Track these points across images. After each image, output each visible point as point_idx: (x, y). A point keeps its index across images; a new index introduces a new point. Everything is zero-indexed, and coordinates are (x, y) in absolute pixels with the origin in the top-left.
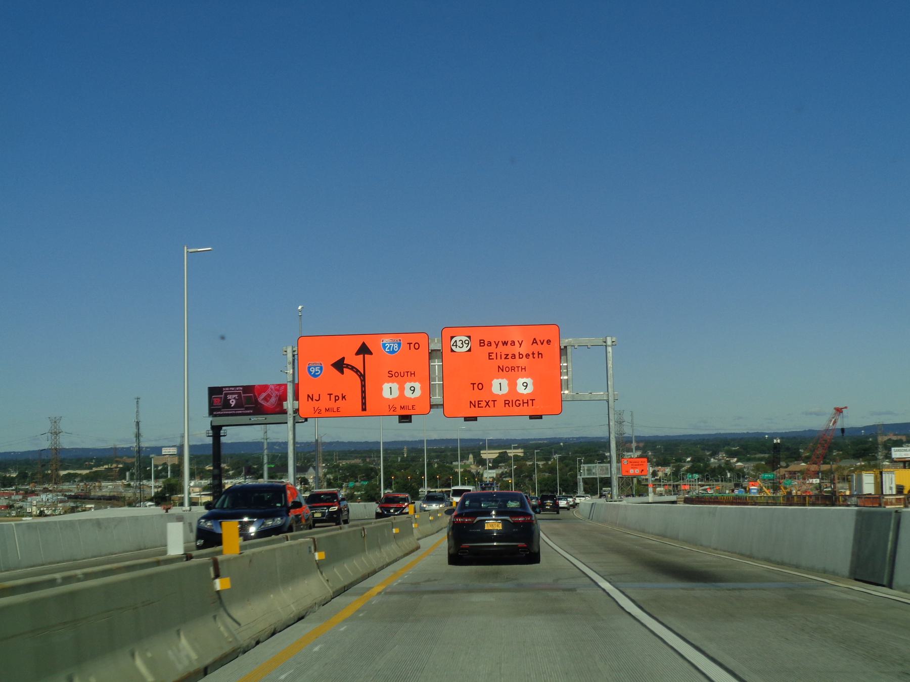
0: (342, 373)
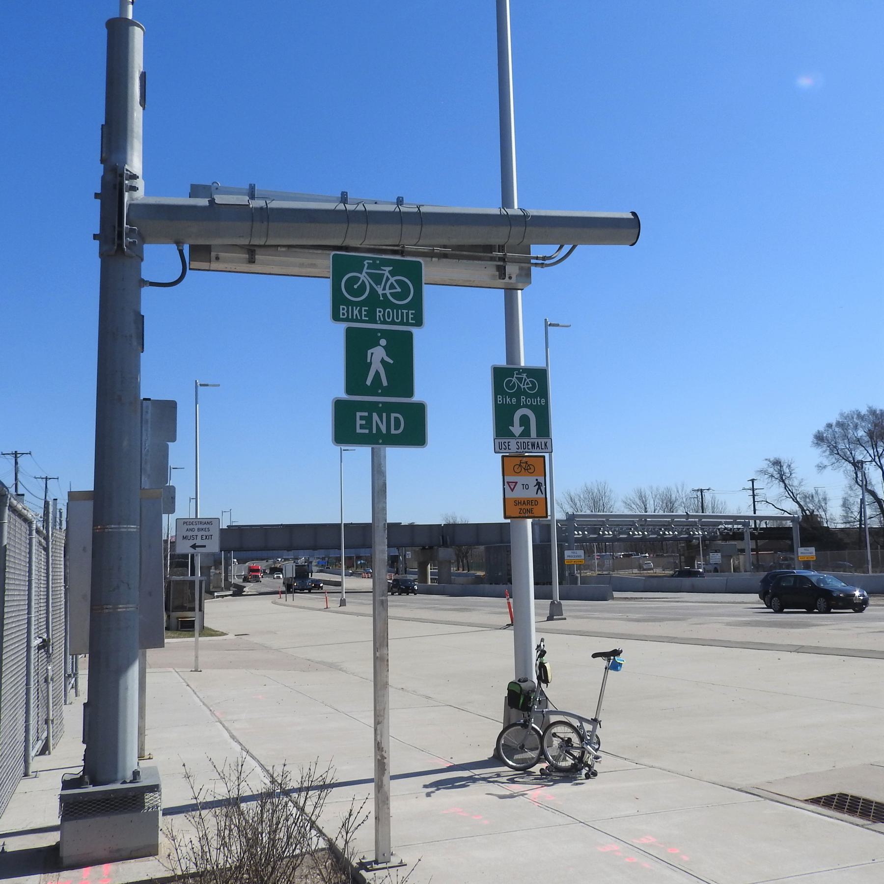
0: (195, 549)
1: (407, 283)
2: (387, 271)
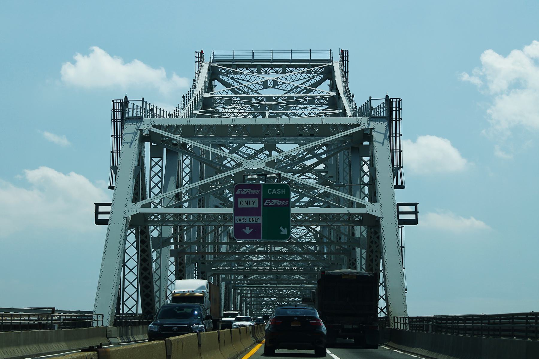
1: (236, 238)
2: (274, 192)
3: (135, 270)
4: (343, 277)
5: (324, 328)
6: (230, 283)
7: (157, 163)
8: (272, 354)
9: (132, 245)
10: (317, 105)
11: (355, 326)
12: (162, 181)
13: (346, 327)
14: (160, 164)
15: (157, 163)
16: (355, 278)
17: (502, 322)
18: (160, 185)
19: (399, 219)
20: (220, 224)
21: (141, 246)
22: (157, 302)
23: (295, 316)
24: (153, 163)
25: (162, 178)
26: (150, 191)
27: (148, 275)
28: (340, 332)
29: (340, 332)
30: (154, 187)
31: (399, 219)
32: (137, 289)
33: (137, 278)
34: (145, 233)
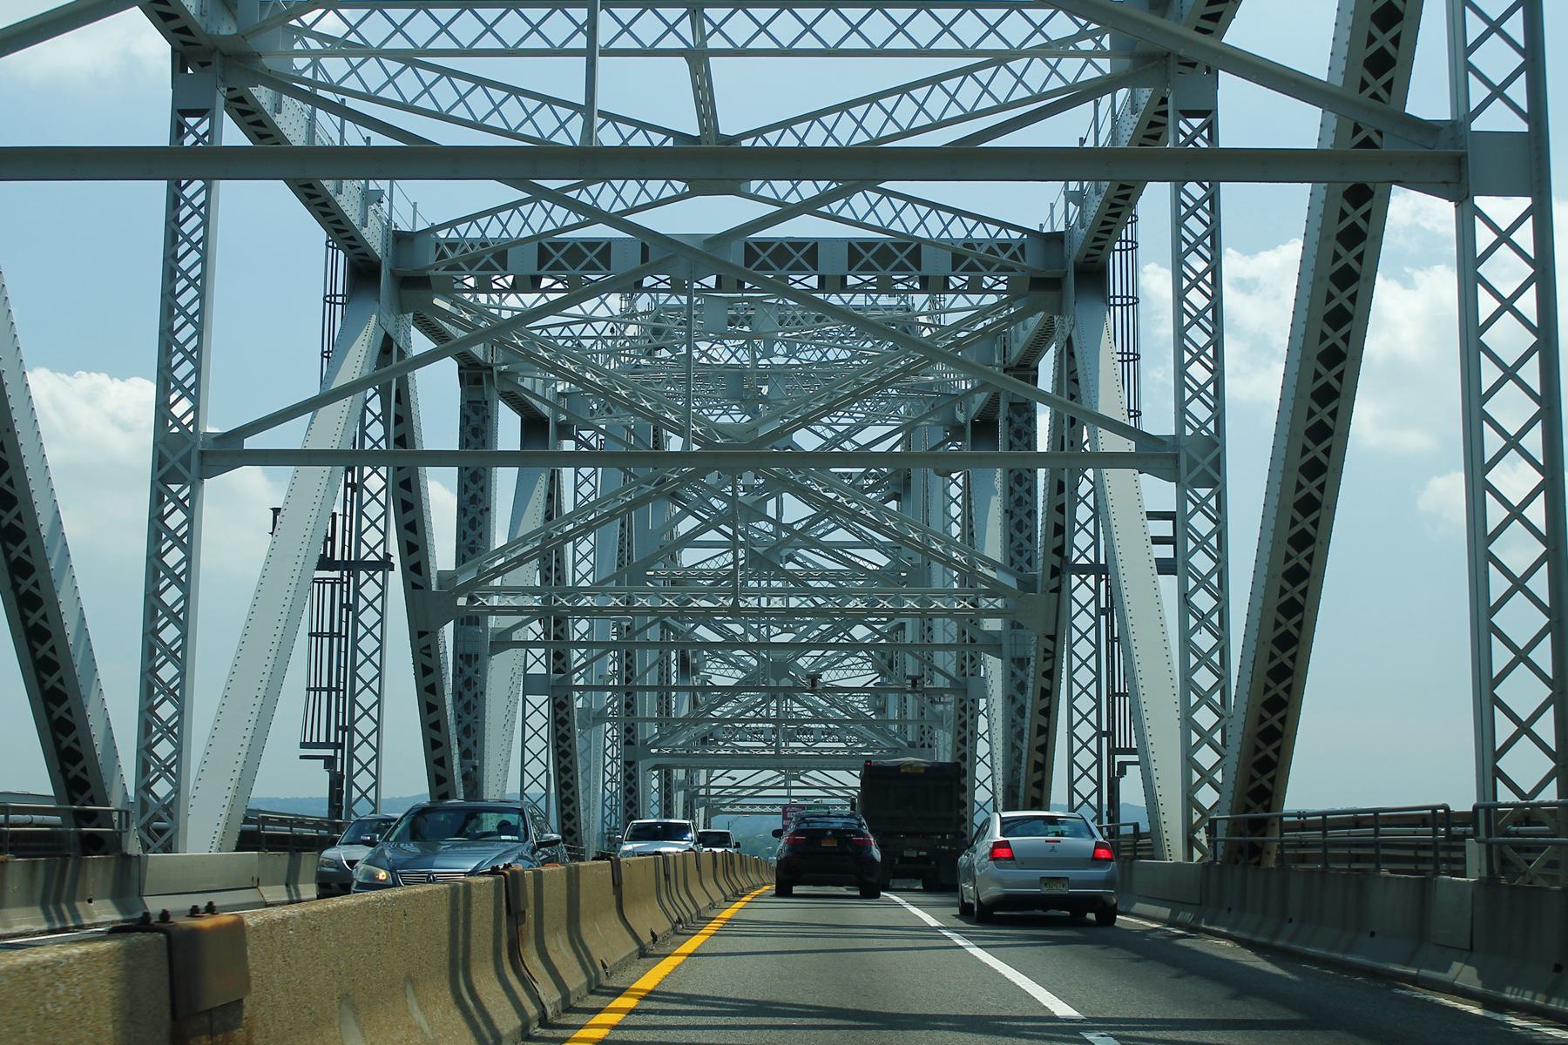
3: (544, 733)
4: (903, 771)
5: (877, 854)
6: (696, 795)
7: (586, 480)
8: (789, 894)
9: (538, 660)
10: (888, 420)
11: (923, 853)
12: (594, 570)
13: (906, 854)
14: (592, 480)
15: (586, 480)
16: (922, 771)
17: (1287, 822)
18: (591, 557)
19: (1172, 546)
20: (861, 279)
21: (554, 664)
22: (610, 664)
23: (827, 830)
24: (580, 480)
25: (595, 488)
26: (574, 569)
27: (571, 797)
28: (897, 863)
29: (897, 863)
30: (581, 561)
31: (1172, 546)
32: (547, 743)
33: (547, 746)
34: (562, 656)
